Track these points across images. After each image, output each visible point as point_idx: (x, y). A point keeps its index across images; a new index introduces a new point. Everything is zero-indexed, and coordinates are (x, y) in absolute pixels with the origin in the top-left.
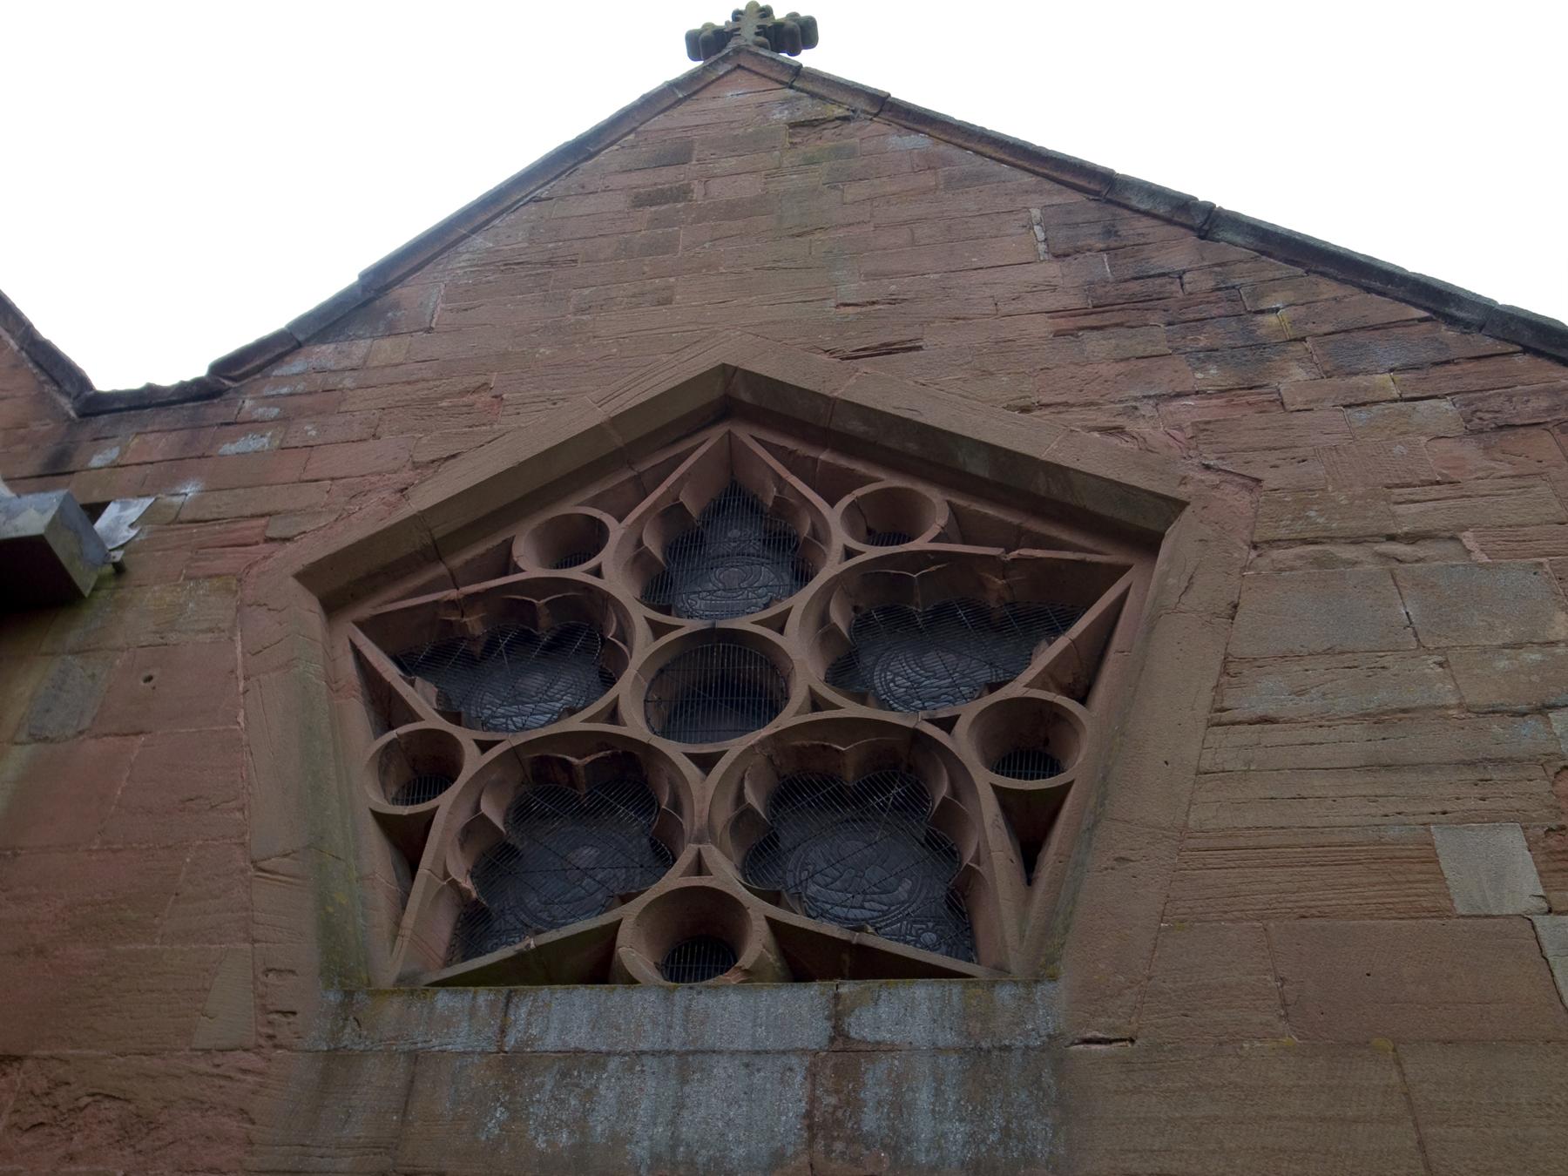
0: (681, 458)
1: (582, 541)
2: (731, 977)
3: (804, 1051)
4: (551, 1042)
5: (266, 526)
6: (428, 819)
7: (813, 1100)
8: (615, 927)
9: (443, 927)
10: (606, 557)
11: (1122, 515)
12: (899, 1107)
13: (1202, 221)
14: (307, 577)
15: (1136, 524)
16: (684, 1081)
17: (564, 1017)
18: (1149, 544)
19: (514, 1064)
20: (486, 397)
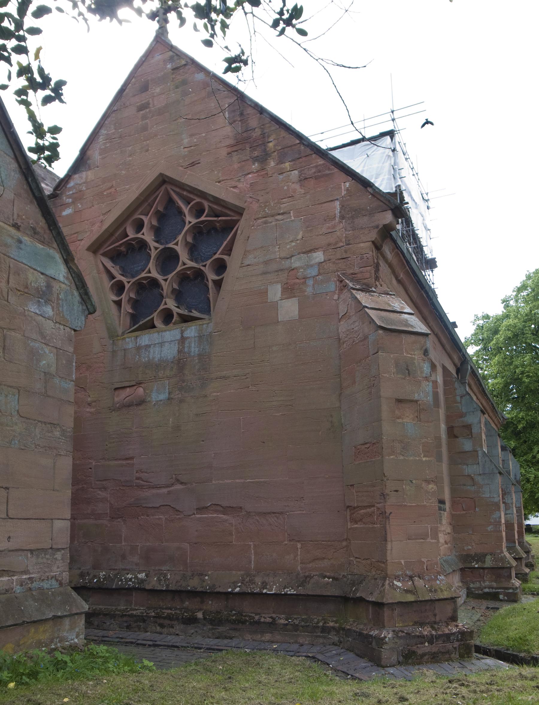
0: (157, 197)
1: (139, 226)
2: (171, 325)
3: (176, 340)
4: (143, 344)
5: (77, 237)
6: (121, 300)
7: (179, 348)
8: (153, 318)
9: (128, 320)
10: (144, 230)
11: (236, 210)
12: (190, 347)
13: (261, 110)
14: (88, 249)
15: (239, 212)
16: (162, 347)
17: (145, 338)
18: (241, 215)
19: (139, 348)
20: (113, 190)
